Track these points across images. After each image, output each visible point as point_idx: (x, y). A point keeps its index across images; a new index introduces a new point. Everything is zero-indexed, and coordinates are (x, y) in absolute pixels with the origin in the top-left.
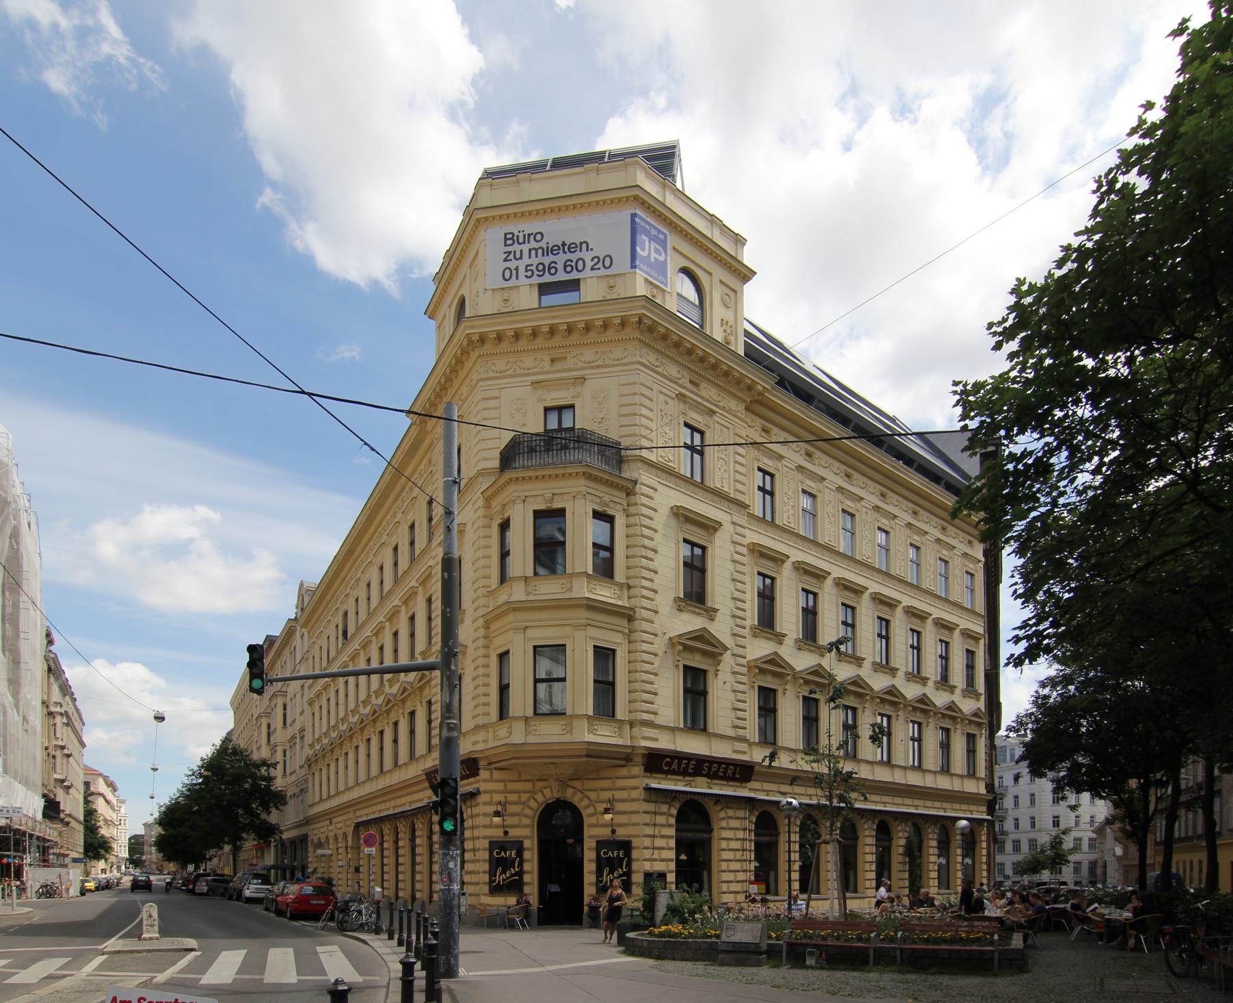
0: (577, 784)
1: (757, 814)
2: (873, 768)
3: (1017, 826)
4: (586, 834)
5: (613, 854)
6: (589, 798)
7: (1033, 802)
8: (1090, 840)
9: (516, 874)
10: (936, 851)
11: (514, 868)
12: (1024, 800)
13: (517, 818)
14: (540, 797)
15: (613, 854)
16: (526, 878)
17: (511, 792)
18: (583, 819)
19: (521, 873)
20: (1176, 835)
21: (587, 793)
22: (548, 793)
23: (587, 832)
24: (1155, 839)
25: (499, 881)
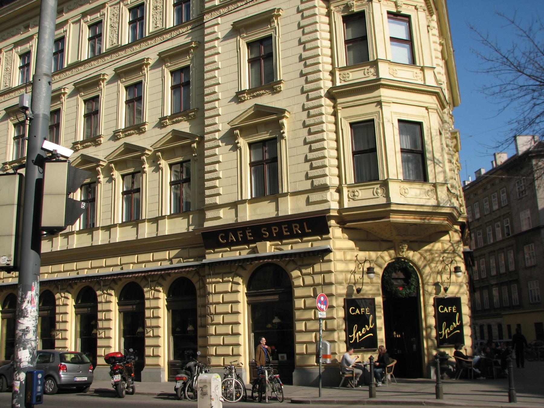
11: (456, 323)
25: (356, 339)
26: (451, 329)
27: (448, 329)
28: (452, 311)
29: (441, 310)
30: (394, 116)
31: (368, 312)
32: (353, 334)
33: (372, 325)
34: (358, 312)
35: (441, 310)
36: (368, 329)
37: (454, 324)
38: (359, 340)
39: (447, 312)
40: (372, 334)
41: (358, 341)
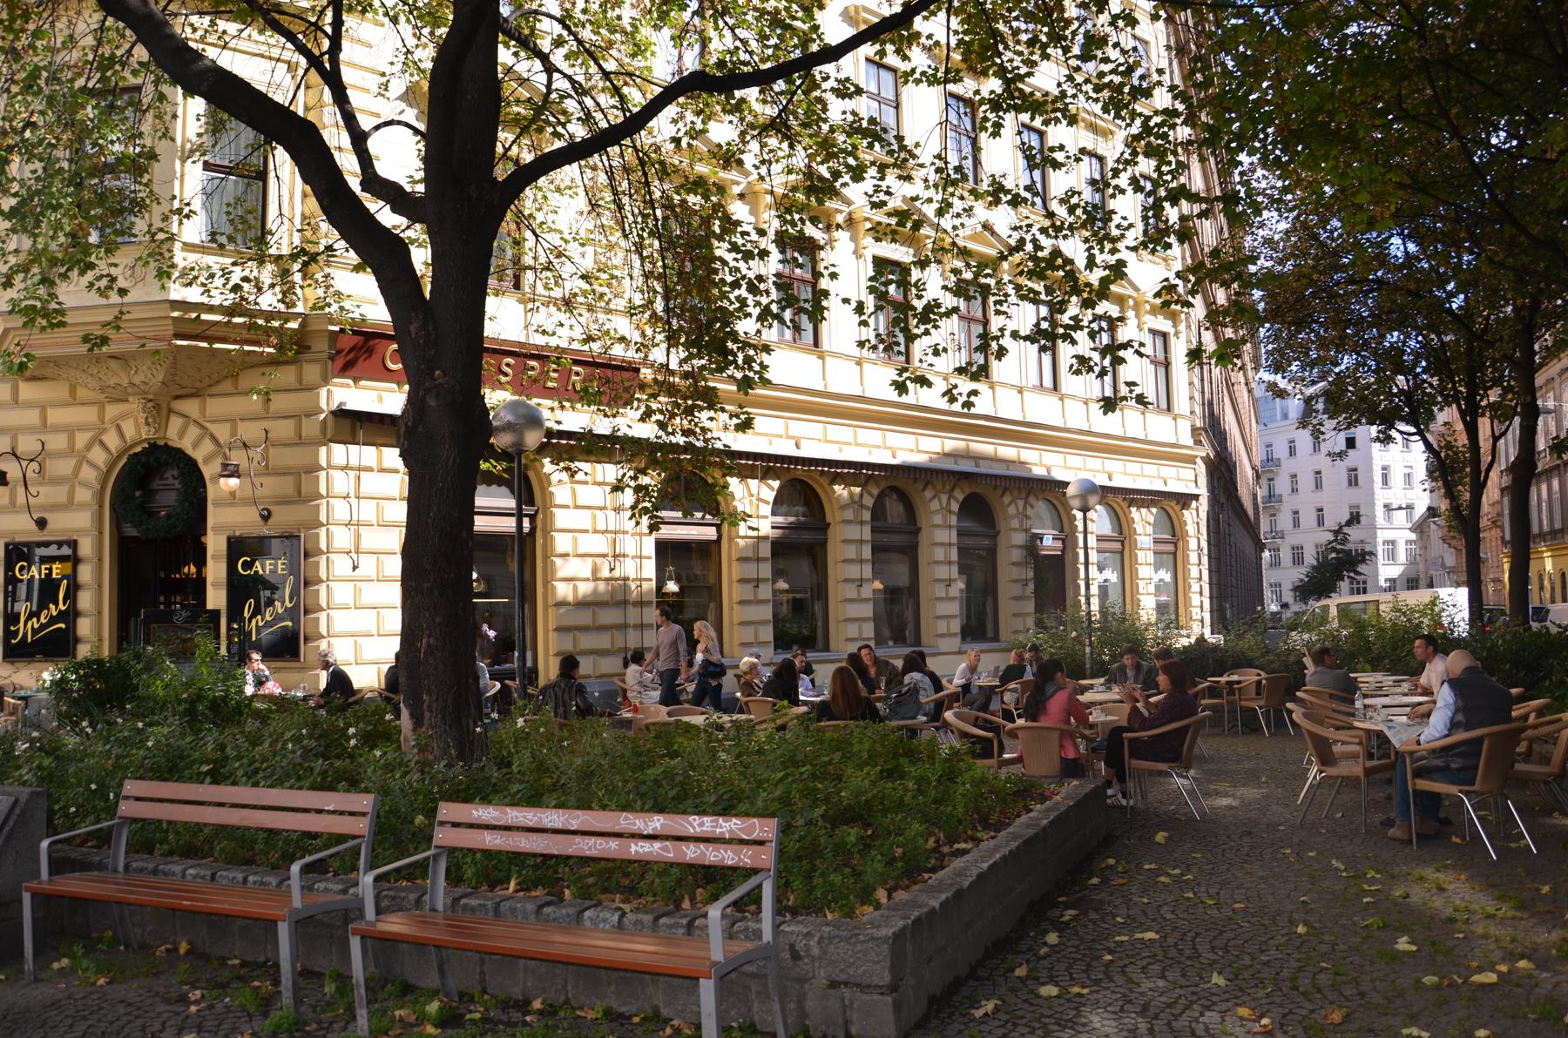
0: (190, 407)
1: (961, 497)
2: (205, 402)
3: (1296, 523)
4: (211, 521)
5: (264, 569)
6: (214, 439)
7: (1318, 485)
8: (1407, 542)
9: (62, 616)
10: (1151, 557)
11: (57, 605)
12: (1305, 481)
13: (65, 488)
14: (112, 440)
15: (264, 569)
16: (84, 627)
17: (58, 429)
18: (204, 486)
19: (71, 615)
20: (1535, 529)
21: (212, 427)
22: (130, 431)
23: (214, 517)
24: (1503, 538)
25: (25, 634)
26: (268, 618)
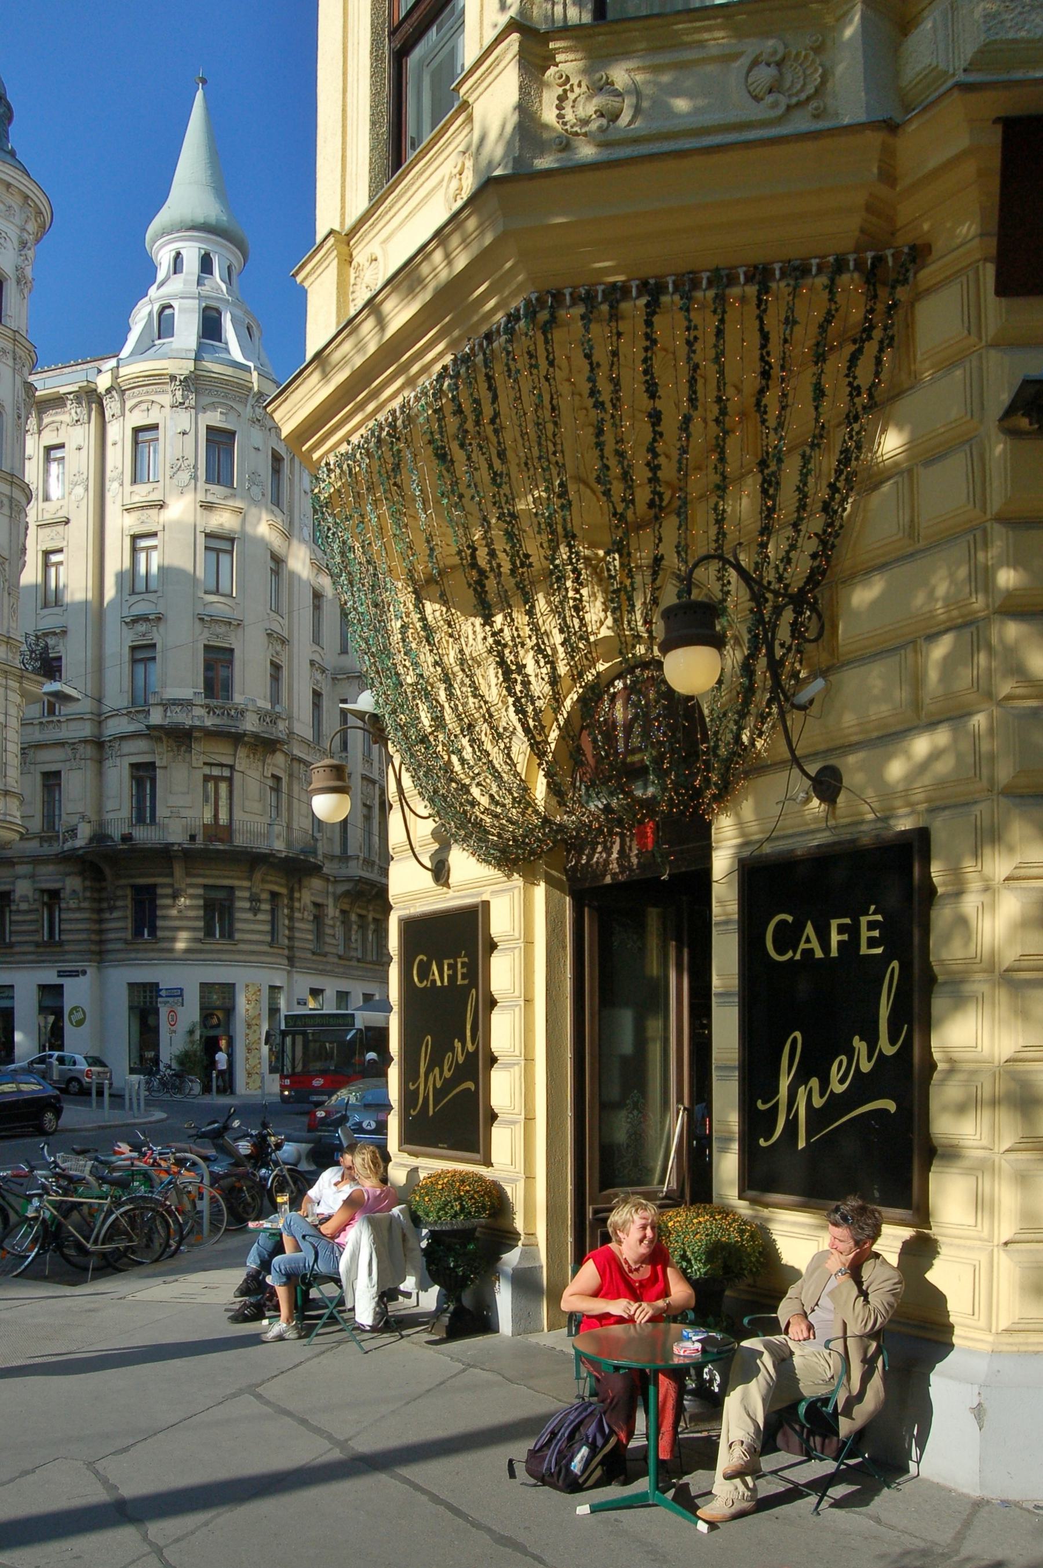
25: (792, 1125)
26: (838, 1088)
27: (814, 1082)
28: (849, 947)
29: (780, 950)
30: (65, 543)
31: (872, 943)
32: (777, 1092)
33: (893, 1041)
34: (815, 944)
35: (780, 950)
36: (866, 1067)
37: (860, 1045)
38: (809, 1135)
39: (819, 954)
40: (891, 1106)
41: (431, 1113)
